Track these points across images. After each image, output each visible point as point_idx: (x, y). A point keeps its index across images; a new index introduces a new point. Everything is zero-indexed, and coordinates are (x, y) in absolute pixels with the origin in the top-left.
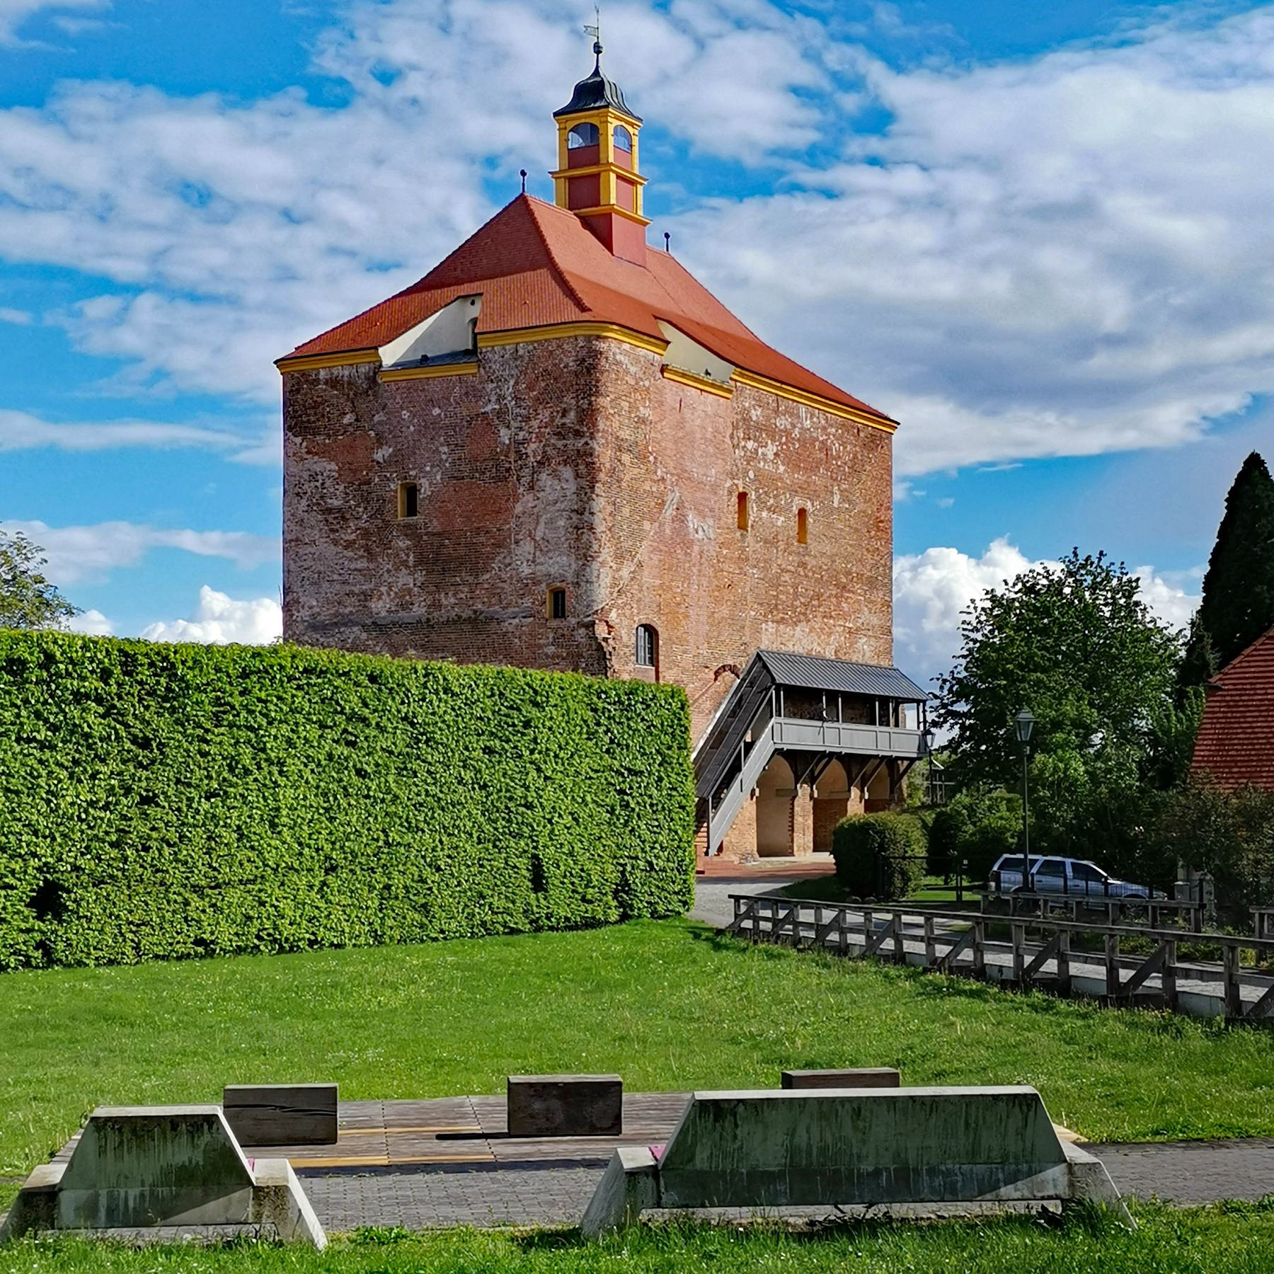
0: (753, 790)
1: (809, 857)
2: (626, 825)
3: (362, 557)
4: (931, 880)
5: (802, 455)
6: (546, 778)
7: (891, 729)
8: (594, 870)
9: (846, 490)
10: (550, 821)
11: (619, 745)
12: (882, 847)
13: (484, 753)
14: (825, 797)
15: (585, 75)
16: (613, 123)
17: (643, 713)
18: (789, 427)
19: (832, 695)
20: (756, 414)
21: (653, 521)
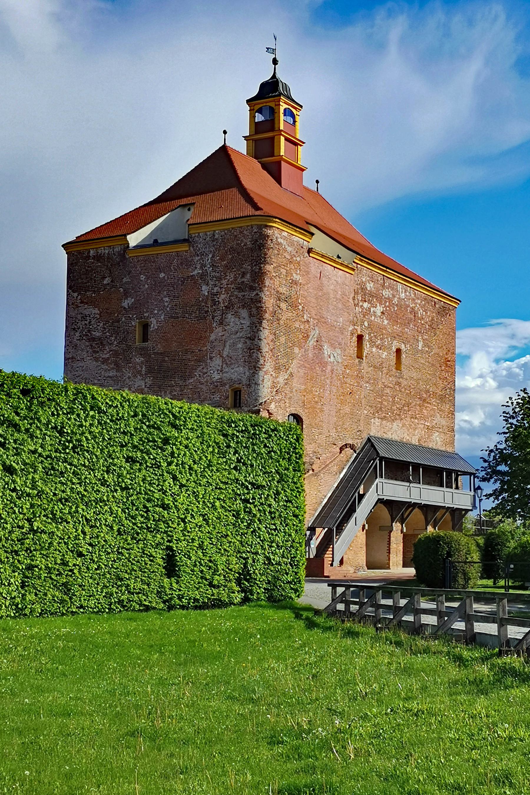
0: (364, 526)
1: (399, 569)
2: (248, 527)
3: (113, 368)
4: (485, 582)
5: (398, 314)
6: (182, 486)
7: (453, 490)
8: (221, 560)
9: (426, 339)
10: (183, 520)
11: (244, 464)
12: (449, 555)
13: (127, 461)
14: (411, 532)
15: (267, 77)
16: (283, 107)
17: (266, 441)
18: (391, 296)
19: (416, 467)
20: (370, 286)
21: (300, 347)
